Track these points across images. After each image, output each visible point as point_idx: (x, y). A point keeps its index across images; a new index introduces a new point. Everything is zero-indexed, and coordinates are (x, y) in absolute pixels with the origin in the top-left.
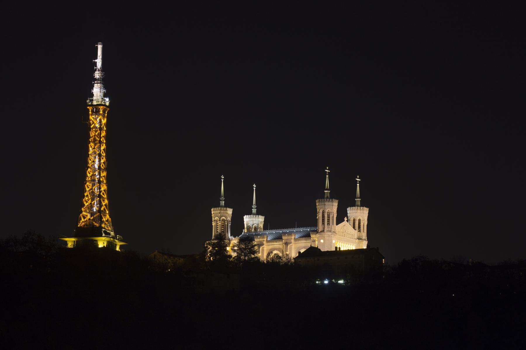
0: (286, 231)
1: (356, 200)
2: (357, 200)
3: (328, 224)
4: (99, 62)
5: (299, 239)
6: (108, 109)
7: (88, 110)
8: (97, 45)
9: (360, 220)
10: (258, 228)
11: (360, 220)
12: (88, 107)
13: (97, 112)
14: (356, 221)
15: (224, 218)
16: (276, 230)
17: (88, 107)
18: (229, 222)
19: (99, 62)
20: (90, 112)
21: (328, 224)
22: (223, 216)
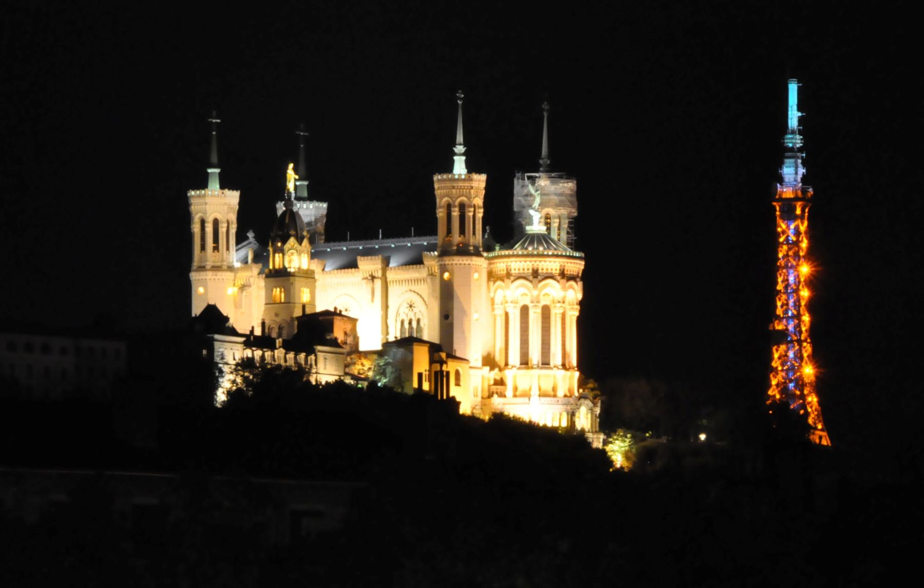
0: (357, 247)
1: (210, 171)
2: (212, 173)
3: (216, 248)
4: (794, 116)
5: (332, 272)
6: (810, 204)
7: (774, 207)
8: (799, 128)
9: (216, 223)
10: (470, 206)
11: (216, 223)
12: (774, 204)
13: (789, 215)
14: (220, 225)
15: (464, 199)
16: (366, 242)
17: (774, 204)
18: (477, 208)
19: (794, 116)
20: (776, 211)
21: (216, 248)
22: (463, 195)
